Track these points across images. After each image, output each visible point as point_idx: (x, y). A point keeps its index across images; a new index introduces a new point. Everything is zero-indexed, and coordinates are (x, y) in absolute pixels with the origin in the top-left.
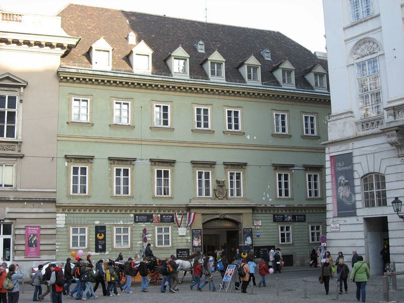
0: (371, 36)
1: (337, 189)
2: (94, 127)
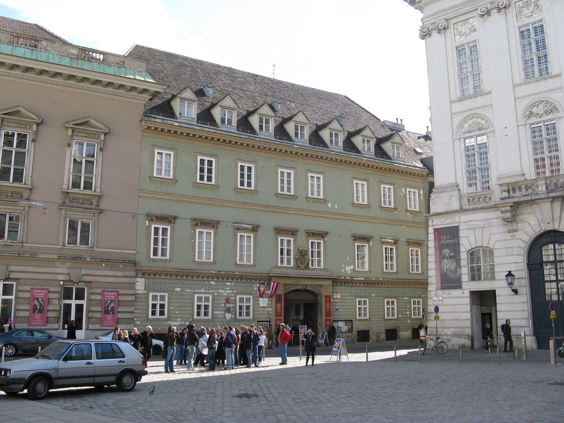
0: (480, 112)
1: (440, 264)
2: (177, 184)
